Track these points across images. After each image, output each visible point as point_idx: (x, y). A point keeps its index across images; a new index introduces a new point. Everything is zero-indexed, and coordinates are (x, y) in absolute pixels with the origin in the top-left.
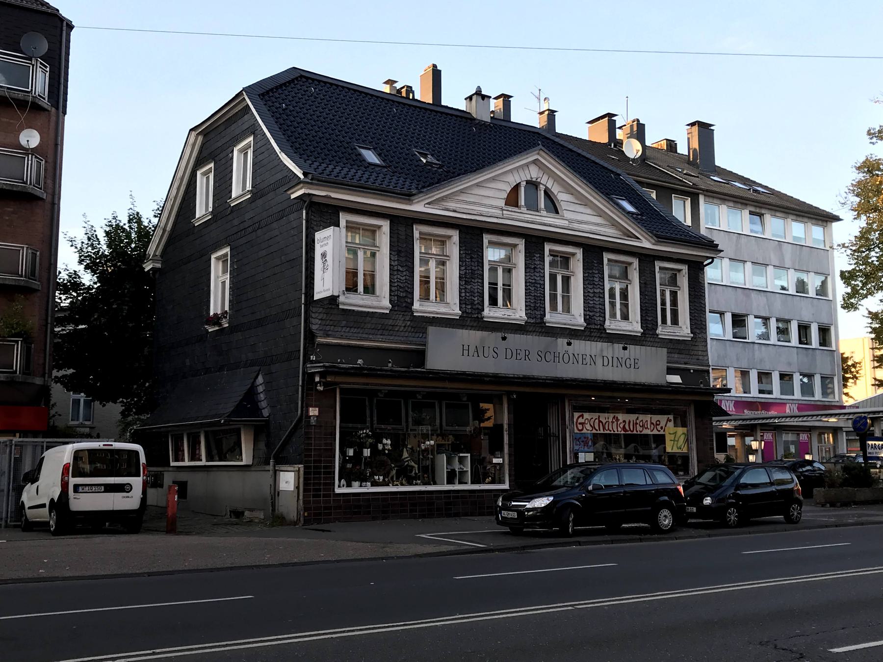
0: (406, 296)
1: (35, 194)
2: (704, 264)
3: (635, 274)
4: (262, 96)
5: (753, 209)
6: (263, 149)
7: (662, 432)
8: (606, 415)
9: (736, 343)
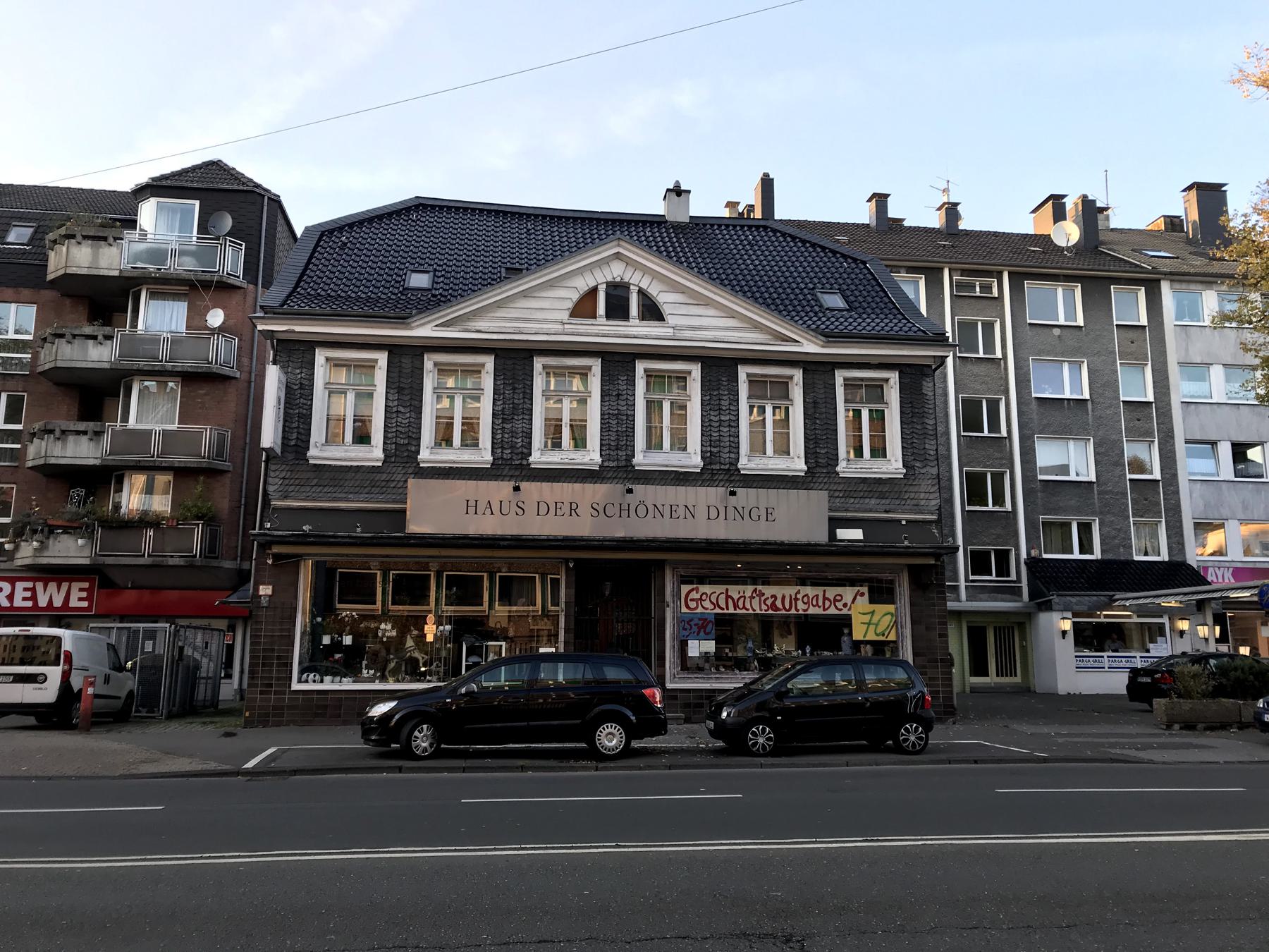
0: (408, 443)
1: (223, 373)
7: (845, 611)
8: (741, 588)
9: (1241, 485)
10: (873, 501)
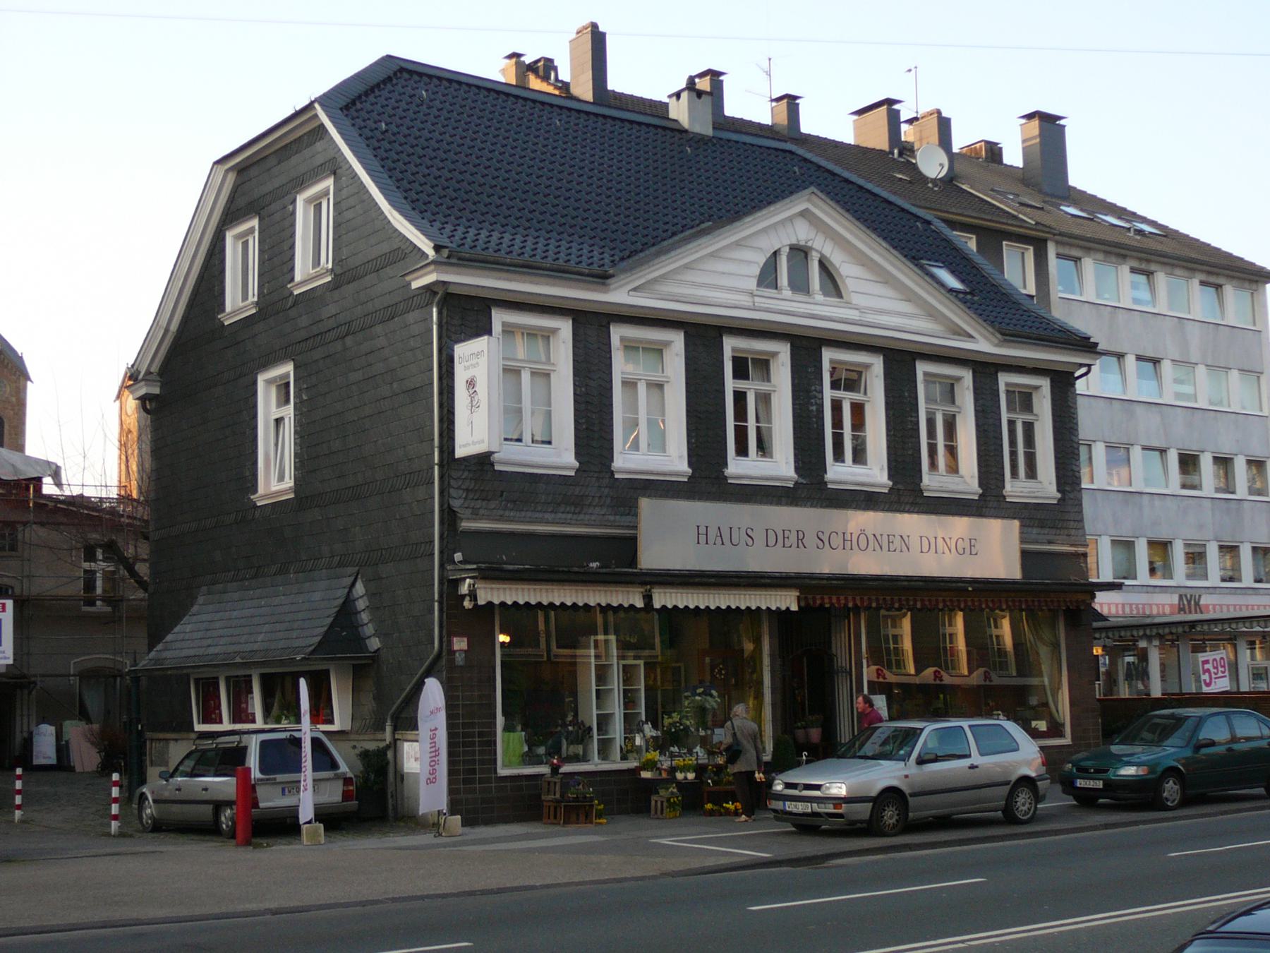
2: (1077, 375)
4: (346, 108)
5: (1135, 264)
10: (1035, 531)
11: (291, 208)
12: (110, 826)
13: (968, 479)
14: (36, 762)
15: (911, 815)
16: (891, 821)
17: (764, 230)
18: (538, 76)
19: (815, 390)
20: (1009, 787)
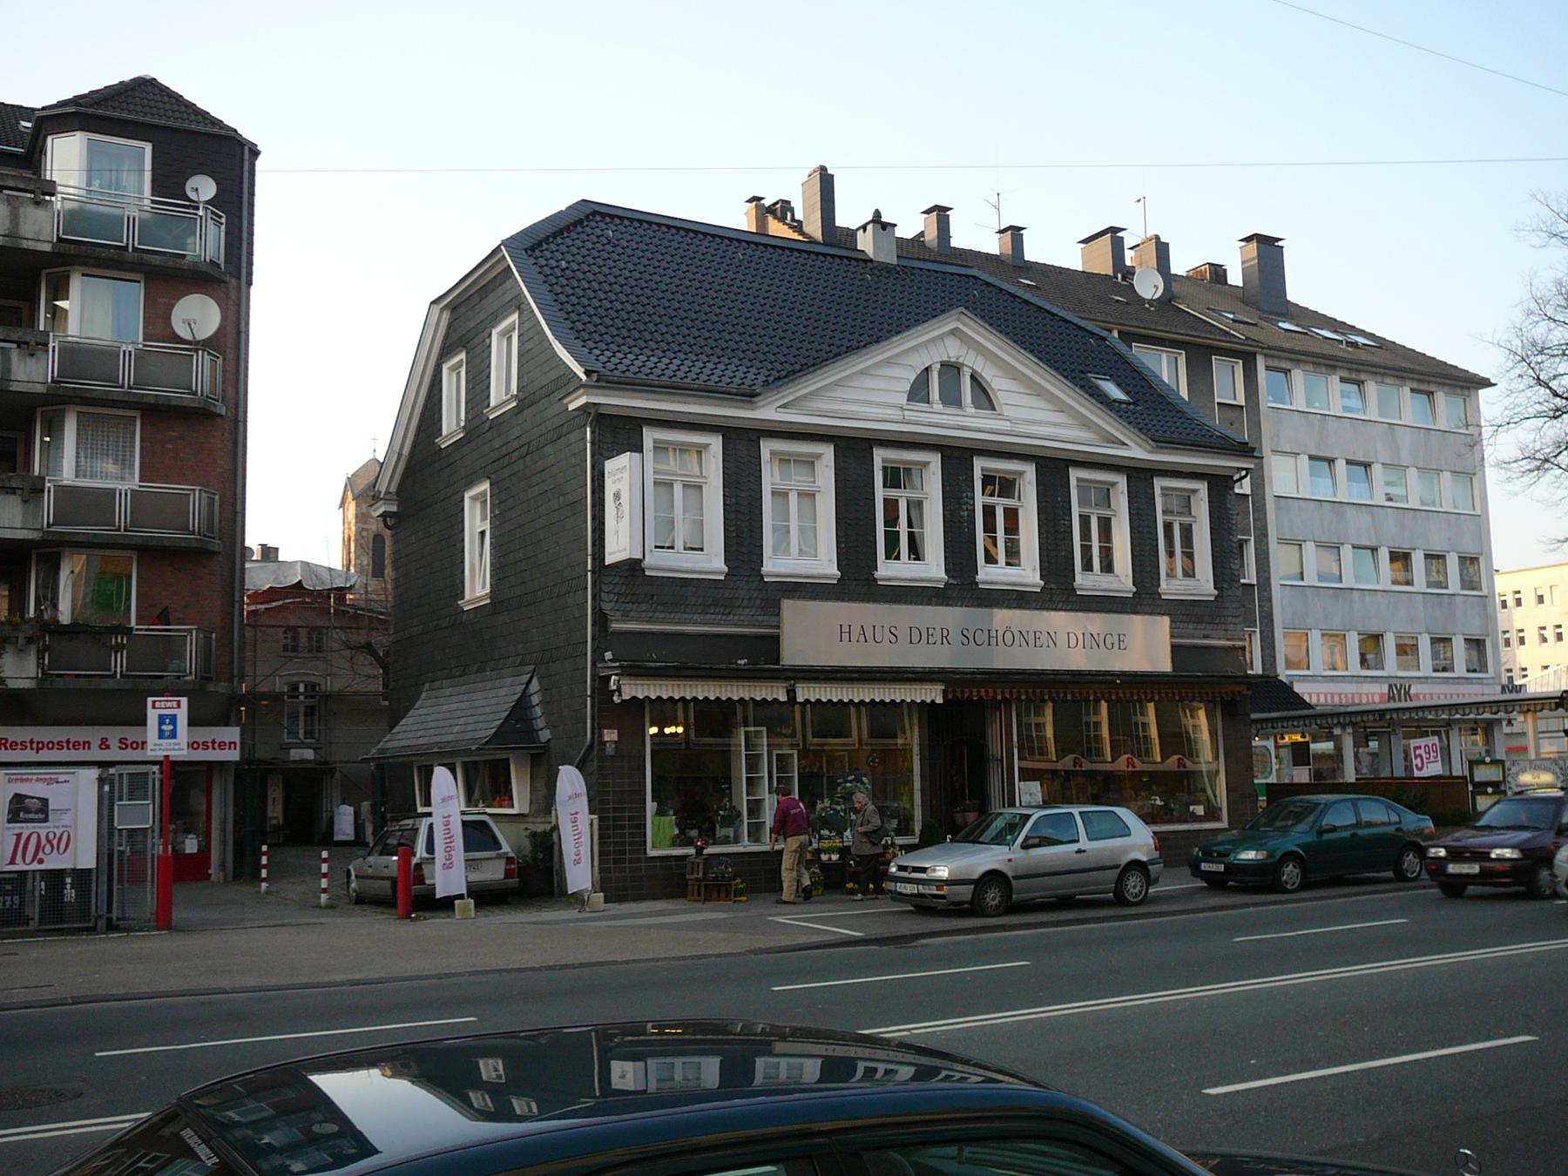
3: (1121, 500)
4: (530, 250)
5: (1345, 374)
6: (530, 334)
10: (1191, 626)
11: (488, 341)
12: (320, 897)
13: (1123, 578)
14: (336, 838)
15: (1014, 896)
16: (994, 903)
17: (915, 348)
18: (775, 217)
19: (967, 497)
20: (1119, 870)
